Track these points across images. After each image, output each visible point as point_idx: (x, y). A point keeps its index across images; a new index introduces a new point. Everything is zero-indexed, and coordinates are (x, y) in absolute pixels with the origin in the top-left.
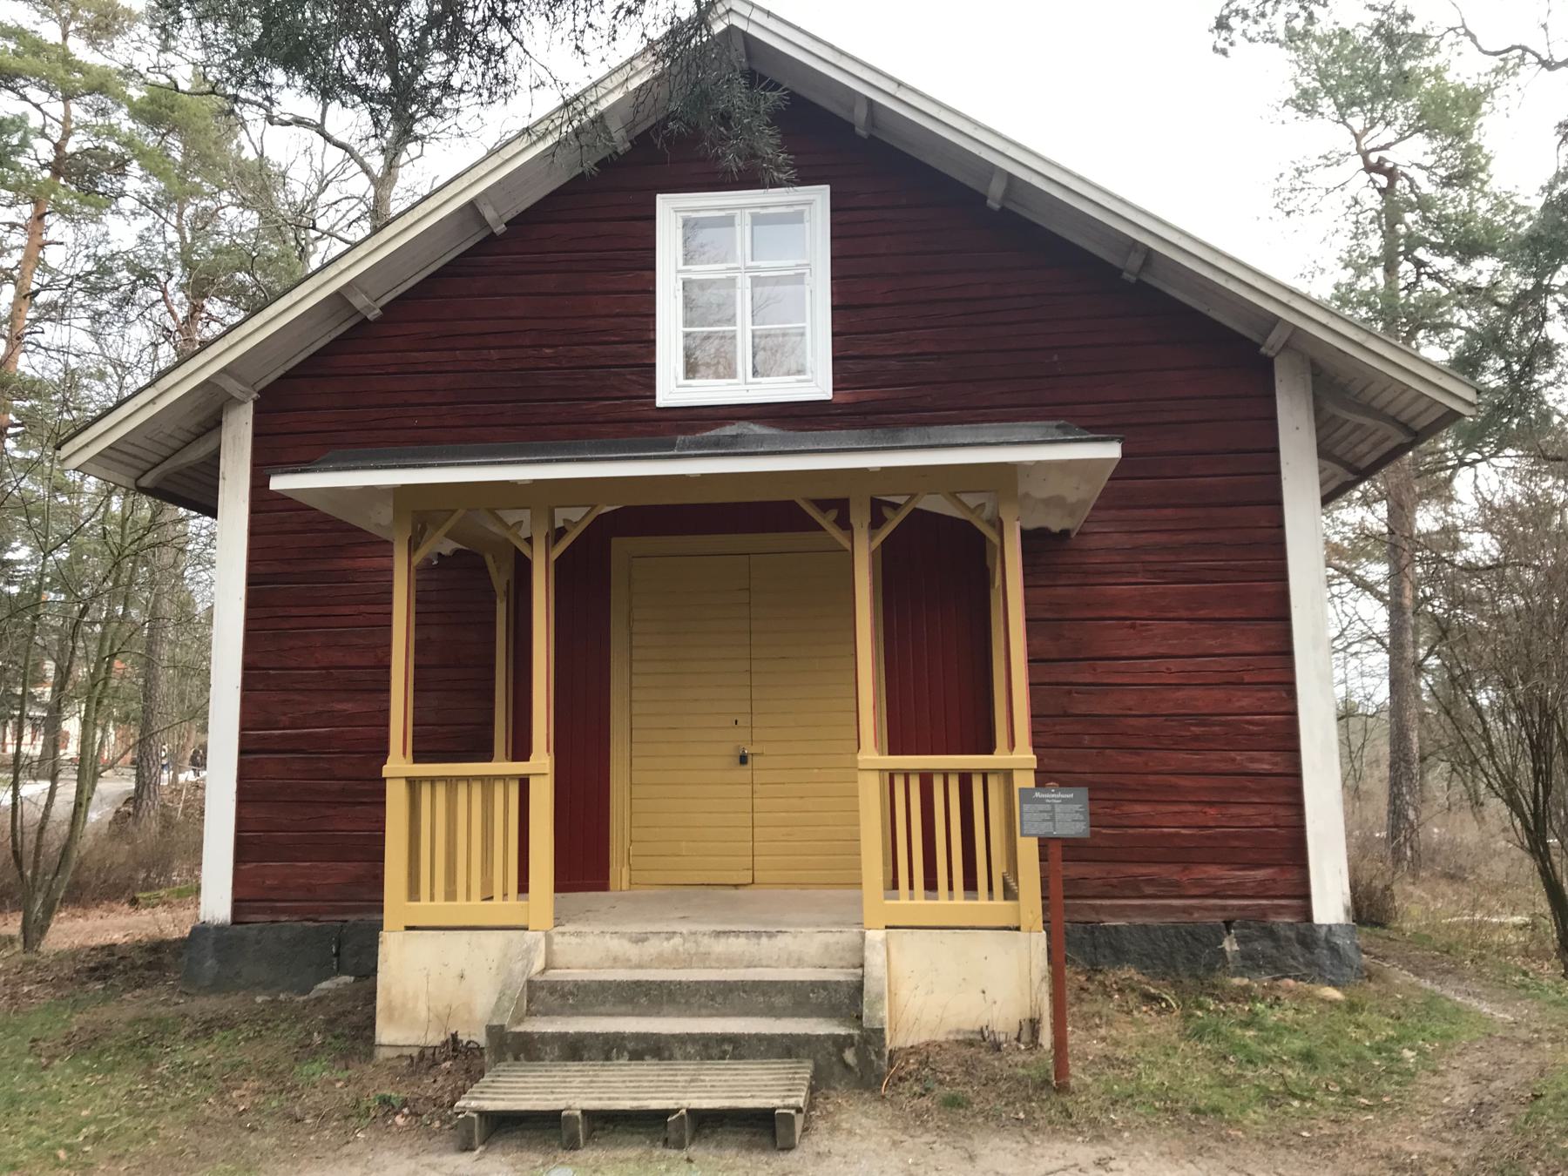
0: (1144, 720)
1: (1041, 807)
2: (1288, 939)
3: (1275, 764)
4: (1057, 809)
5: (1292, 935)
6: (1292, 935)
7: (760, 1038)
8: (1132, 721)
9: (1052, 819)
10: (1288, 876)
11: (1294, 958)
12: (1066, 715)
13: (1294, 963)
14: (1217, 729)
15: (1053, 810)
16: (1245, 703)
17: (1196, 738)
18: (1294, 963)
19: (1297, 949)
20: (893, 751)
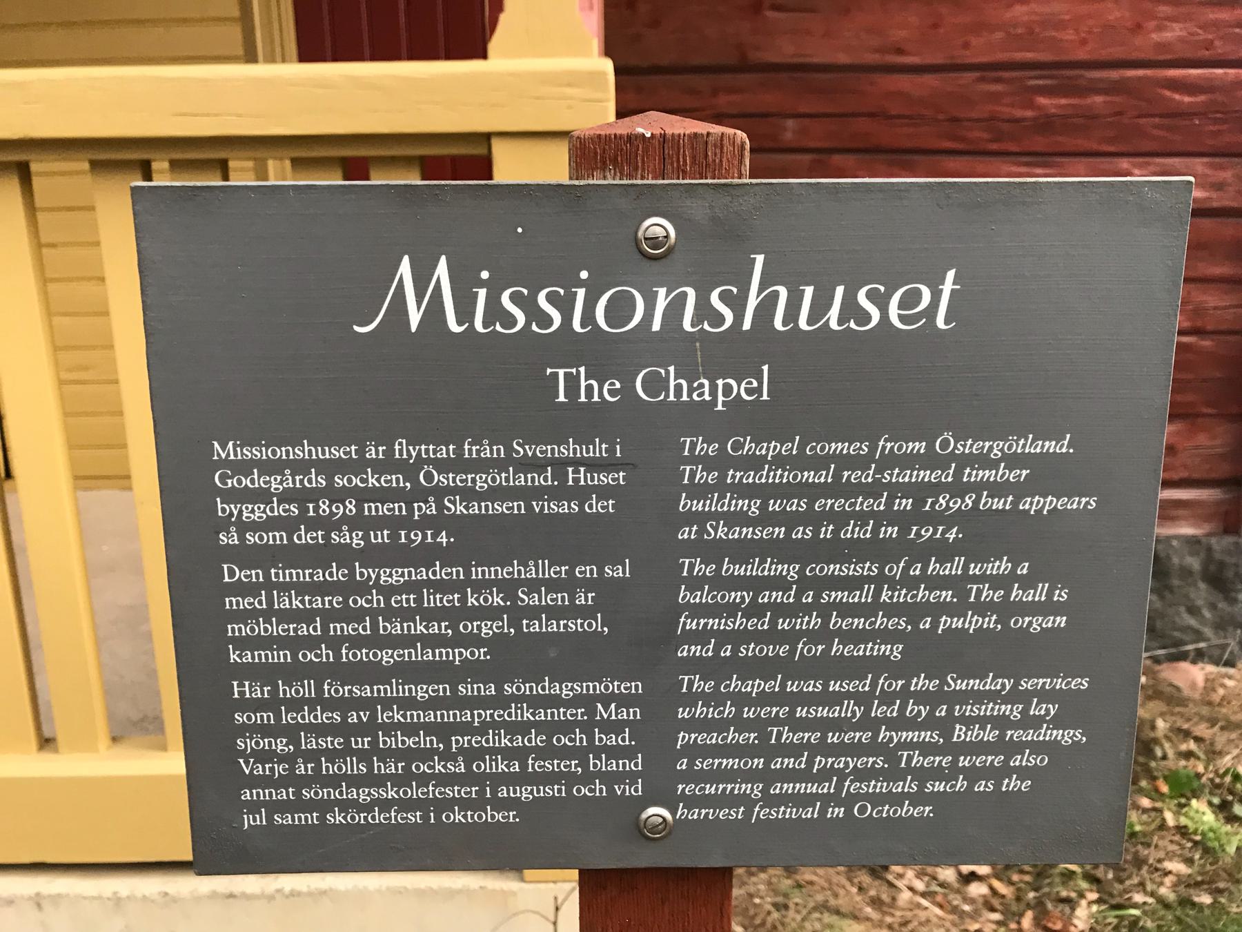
0: (930, 80)
1: (481, 477)
2: (1186, 572)
3: (1219, 186)
4: (712, 508)
5: (1195, 563)
6: (1195, 563)
7: (653, 316)
8: (904, 82)
9: (641, 639)
10: (1202, 439)
11: (1193, 611)
12: (744, 66)
13: (1192, 622)
14: (1099, 99)
15: (647, 523)
16: (1174, 33)
17: (1046, 124)
18: (1192, 622)
19: (1201, 593)
20: (423, 179)
